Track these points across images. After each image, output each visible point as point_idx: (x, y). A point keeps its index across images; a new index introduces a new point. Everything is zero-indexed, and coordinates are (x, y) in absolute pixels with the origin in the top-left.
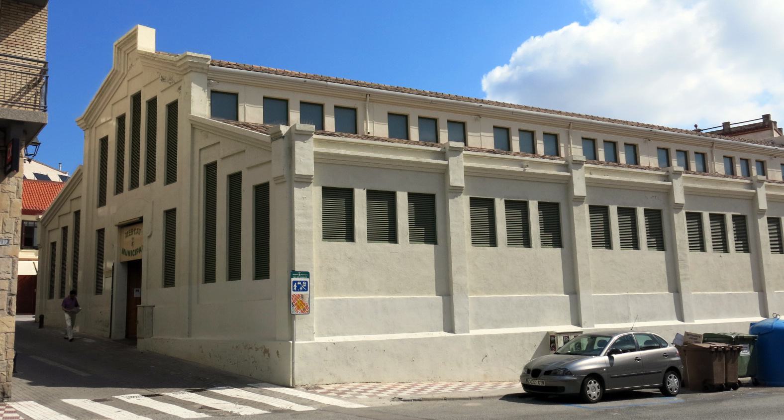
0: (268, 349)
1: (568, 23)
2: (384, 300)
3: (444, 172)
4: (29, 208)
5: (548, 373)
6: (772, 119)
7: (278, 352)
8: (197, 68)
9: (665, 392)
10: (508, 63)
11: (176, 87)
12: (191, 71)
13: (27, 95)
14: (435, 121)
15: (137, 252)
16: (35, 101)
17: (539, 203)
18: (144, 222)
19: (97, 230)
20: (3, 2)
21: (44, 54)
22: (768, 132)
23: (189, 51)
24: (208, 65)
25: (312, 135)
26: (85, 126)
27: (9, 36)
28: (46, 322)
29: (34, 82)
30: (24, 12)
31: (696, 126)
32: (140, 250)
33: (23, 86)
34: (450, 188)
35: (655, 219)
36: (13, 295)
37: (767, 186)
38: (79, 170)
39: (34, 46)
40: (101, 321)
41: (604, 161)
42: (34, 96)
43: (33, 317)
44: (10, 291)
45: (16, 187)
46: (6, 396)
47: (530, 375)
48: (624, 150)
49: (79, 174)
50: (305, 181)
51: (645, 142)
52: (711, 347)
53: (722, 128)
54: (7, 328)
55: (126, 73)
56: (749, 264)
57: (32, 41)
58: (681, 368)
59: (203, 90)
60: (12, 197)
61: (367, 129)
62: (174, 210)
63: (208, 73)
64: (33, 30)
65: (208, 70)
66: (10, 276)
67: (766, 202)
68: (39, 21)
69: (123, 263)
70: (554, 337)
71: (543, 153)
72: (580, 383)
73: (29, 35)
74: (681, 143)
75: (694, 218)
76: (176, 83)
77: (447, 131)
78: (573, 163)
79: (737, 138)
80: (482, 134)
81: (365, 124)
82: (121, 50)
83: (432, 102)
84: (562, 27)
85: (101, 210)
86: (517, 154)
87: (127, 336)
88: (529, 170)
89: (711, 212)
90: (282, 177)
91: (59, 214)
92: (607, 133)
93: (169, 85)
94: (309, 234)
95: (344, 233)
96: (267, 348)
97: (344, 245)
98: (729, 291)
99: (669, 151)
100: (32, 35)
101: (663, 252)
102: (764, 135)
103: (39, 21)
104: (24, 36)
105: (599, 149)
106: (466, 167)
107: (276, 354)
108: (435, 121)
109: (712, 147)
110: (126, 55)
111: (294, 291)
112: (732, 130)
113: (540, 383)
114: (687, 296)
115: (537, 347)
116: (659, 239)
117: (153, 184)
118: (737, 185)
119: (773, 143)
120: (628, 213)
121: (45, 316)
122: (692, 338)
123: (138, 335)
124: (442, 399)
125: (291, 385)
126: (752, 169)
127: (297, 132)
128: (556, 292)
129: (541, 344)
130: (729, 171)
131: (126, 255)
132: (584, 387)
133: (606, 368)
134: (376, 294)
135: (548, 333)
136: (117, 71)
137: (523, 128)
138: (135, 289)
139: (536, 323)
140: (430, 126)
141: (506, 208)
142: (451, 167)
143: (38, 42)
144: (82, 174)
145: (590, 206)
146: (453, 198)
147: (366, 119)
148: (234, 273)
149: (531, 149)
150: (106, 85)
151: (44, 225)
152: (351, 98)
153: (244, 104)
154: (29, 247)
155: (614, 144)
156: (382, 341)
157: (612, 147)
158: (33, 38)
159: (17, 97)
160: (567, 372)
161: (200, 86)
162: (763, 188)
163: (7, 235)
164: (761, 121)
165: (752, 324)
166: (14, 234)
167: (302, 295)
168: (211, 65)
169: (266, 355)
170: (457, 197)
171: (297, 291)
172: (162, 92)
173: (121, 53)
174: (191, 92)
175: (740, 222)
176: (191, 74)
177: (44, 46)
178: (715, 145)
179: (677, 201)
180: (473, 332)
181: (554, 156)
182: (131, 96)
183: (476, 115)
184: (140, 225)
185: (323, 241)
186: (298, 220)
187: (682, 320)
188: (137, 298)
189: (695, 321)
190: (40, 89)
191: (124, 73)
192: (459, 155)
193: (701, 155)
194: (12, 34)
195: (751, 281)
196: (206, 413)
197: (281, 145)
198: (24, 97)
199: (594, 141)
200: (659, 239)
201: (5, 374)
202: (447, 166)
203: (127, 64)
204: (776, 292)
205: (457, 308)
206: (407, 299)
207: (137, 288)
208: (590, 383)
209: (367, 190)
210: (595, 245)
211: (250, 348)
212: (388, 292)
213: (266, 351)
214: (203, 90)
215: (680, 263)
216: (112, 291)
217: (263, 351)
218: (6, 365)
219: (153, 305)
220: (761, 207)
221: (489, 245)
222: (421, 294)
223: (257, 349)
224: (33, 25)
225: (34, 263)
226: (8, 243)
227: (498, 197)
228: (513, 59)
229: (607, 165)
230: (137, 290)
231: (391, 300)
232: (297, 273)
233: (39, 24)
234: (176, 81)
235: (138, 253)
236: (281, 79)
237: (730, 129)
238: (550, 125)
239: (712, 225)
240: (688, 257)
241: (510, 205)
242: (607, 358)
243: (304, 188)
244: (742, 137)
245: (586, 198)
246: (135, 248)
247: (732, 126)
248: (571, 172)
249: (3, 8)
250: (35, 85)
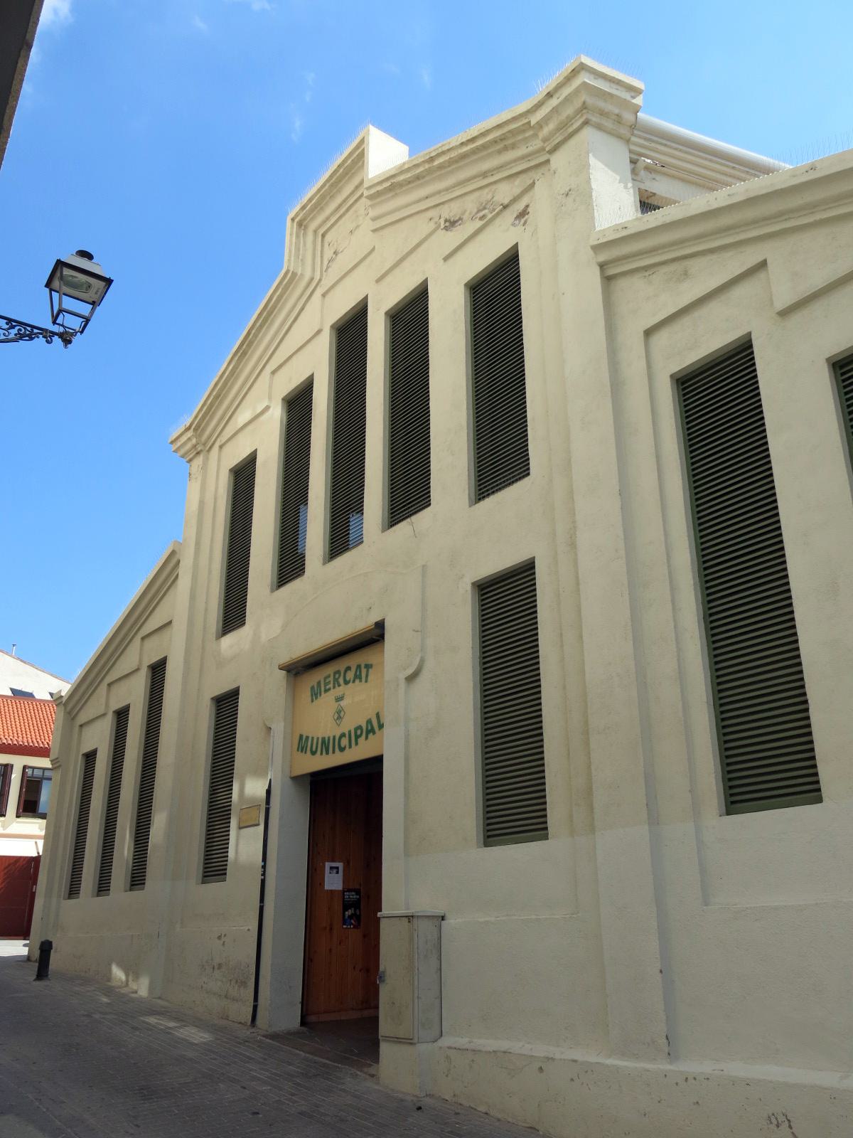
4: (37, 745)
11: (510, 215)
15: (357, 737)
19: (212, 699)
26: (194, 446)
28: (55, 959)
32: (372, 728)
38: (173, 553)
40: (220, 966)
43: (25, 945)
49: (174, 561)
55: (317, 277)
62: (526, 571)
63: (634, 139)
69: (296, 779)
76: (505, 207)
82: (306, 227)
85: (228, 641)
87: (303, 1023)
91: (108, 679)
93: (482, 223)
110: (320, 238)
117: (422, 519)
121: (54, 945)
123: (385, 1028)
131: (314, 753)
136: (294, 274)
138: (328, 865)
144: (179, 562)
150: (258, 324)
151: (69, 713)
154: (30, 814)
161: (615, 170)
173: (305, 234)
176: (588, 133)
182: (332, 327)
184: (376, 647)
188: (332, 891)
191: (312, 279)
203: (322, 257)
207: (333, 861)
216: (264, 867)
219: (439, 912)
225: (36, 843)
230: (332, 868)
234: (506, 202)
235: (362, 740)
246: (348, 725)
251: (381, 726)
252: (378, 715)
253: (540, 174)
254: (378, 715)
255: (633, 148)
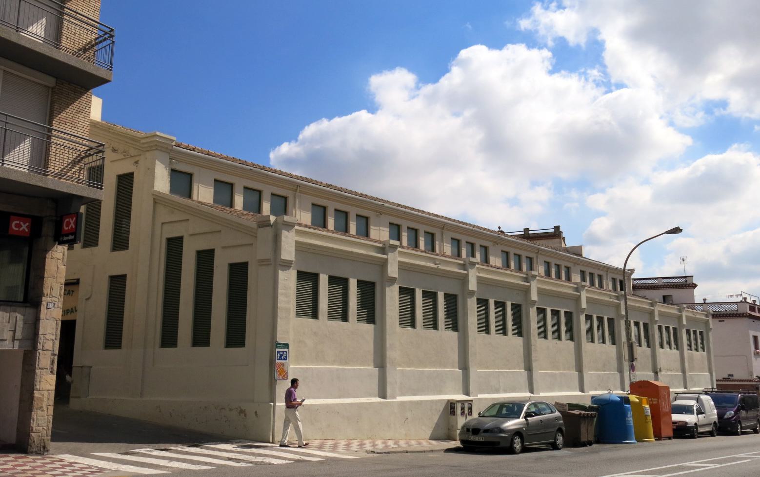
0: (245, 410)
1: (359, 109)
2: (338, 370)
3: (384, 264)
5: (486, 431)
6: (561, 230)
7: (256, 412)
8: (162, 147)
9: (555, 447)
10: (296, 140)
12: (157, 149)
13: (73, 170)
14: (231, 185)
15: (67, 313)
16: (79, 175)
17: (445, 294)
18: (80, 284)
20: (58, 82)
21: (88, 133)
22: (557, 240)
23: (158, 131)
24: (172, 146)
25: (294, 226)
27: (62, 114)
29: (79, 158)
30: (73, 93)
31: (499, 228)
33: (70, 161)
34: (389, 278)
35: (368, 291)
36: (55, 355)
37: (587, 291)
39: (81, 125)
41: (450, 255)
42: (78, 171)
44: (53, 351)
45: (62, 254)
46: (46, 449)
47: (471, 433)
48: (334, 216)
50: (287, 265)
51: (377, 216)
52: (580, 414)
53: (523, 233)
54: (50, 386)
56: (573, 350)
57: (79, 120)
58: (564, 428)
59: (165, 168)
60: (58, 264)
61: (443, 251)
63: (171, 153)
64: (81, 111)
65: (172, 150)
66: (53, 337)
67: (586, 302)
68: (85, 102)
70: (454, 404)
71: (354, 234)
72: (510, 439)
73: (78, 114)
74: (530, 251)
75: (407, 292)
77: (355, 223)
78: (469, 264)
79: (532, 242)
80: (381, 228)
81: (294, 211)
83: (347, 197)
84: (351, 114)
86: (331, 232)
88: (441, 267)
89: (552, 308)
90: (268, 260)
92: (412, 221)
93: (123, 157)
94: (288, 310)
95: (310, 311)
96: (243, 408)
97: (310, 321)
98: (560, 371)
99: (560, 267)
100: (80, 115)
101: (522, 338)
102: (554, 242)
103: (85, 102)
104: (72, 115)
105: (463, 248)
106: (399, 262)
107: (254, 415)
108: (231, 185)
109: (538, 253)
111: (278, 359)
112: (531, 236)
113: (480, 439)
114: (537, 373)
115: (441, 412)
116: (455, 322)
118: (513, 278)
119: (567, 251)
120: (430, 295)
122: (560, 407)
124: (404, 452)
125: (271, 441)
126: (349, 223)
127: (284, 223)
128: (453, 367)
129: (443, 409)
130: (518, 268)
132: (512, 442)
133: (525, 427)
134: (332, 364)
135: (448, 401)
137: (454, 237)
139: (440, 392)
140: (343, 217)
141: (330, 283)
142: (390, 261)
143: (83, 121)
145: (477, 299)
146: (389, 286)
147: (295, 207)
148: (201, 338)
149: (322, 222)
152: (283, 187)
153: (198, 184)
155: (416, 231)
156: (337, 404)
157: (414, 233)
158: (80, 118)
159: (65, 170)
160: (502, 431)
162: (535, 281)
163: (53, 299)
164: (553, 230)
165: (593, 397)
166: (58, 298)
167: (283, 364)
168: (175, 146)
169: (242, 415)
170: (392, 286)
171: (280, 360)
172: (111, 161)
174: (154, 169)
175: (517, 309)
177: (88, 126)
178: (609, 271)
179: (471, 288)
180: (400, 399)
181: (322, 227)
183: (377, 212)
185: (296, 317)
186: (281, 298)
187: (532, 392)
189: (541, 393)
190: (83, 165)
192: (395, 251)
193: (470, 245)
194: (64, 112)
195: (574, 364)
196: (168, 471)
197: (268, 232)
198: (70, 172)
199: (346, 214)
200: (455, 322)
201: (46, 429)
202: (387, 260)
204: (589, 372)
205: (389, 379)
206: (354, 369)
208: (516, 439)
209: (329, 276)
210: (300, 313)
211: (222, 409)
212: (341, 363)
213: (242, 411)
214: (165, 168)
215: (533, 348)
217: (238, 411)
218: (46, 420)
219: (90, 366)
220: (471, 288)
221: (410, 327)
222: (364, 365)
223: (231, 410)
224: (80, 106)
226: (54, 306)
227: (419, 288)
228: (301, 137)
229: (426, 252)
231: (343, 370)
232: (280, 344)
233: (85, 105)
234: (132, 155)
235: (69, 314)
236: (231, 165)
237: (529, 234)
238: (431, 225)
239: (424, 303)
240: (538, 344)
241: (333, 280)
242: (524, 419)
243: (286, 270)
244: (539, 242)
245: (293, 262)
247: (530, 232)
248: (468, 271)
249: (57, 87)
250: (79, 161)
251: (76, 311)
252: (75, 308)
253: (35, 410)
254: (75, 308)
255: (171, 155)
